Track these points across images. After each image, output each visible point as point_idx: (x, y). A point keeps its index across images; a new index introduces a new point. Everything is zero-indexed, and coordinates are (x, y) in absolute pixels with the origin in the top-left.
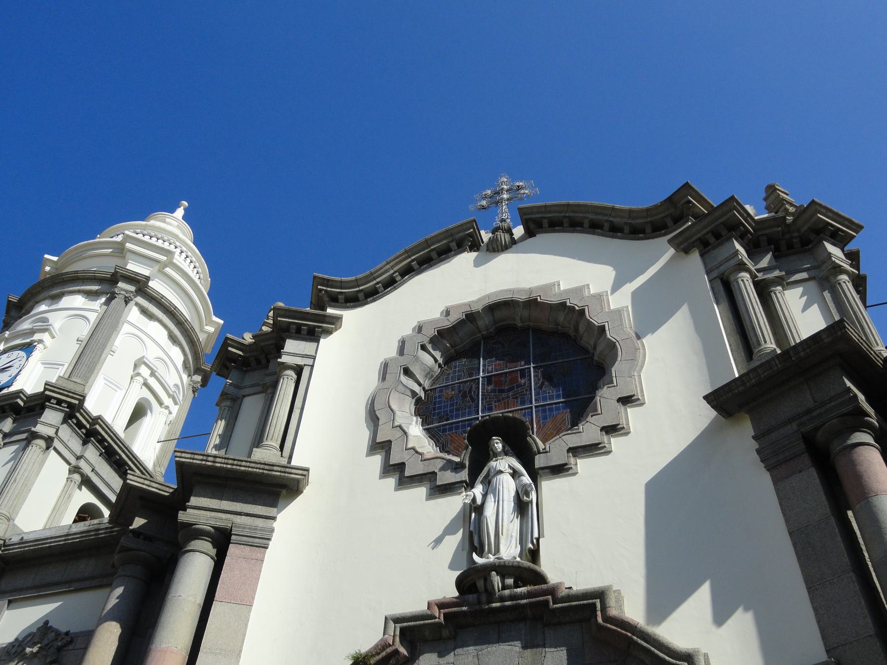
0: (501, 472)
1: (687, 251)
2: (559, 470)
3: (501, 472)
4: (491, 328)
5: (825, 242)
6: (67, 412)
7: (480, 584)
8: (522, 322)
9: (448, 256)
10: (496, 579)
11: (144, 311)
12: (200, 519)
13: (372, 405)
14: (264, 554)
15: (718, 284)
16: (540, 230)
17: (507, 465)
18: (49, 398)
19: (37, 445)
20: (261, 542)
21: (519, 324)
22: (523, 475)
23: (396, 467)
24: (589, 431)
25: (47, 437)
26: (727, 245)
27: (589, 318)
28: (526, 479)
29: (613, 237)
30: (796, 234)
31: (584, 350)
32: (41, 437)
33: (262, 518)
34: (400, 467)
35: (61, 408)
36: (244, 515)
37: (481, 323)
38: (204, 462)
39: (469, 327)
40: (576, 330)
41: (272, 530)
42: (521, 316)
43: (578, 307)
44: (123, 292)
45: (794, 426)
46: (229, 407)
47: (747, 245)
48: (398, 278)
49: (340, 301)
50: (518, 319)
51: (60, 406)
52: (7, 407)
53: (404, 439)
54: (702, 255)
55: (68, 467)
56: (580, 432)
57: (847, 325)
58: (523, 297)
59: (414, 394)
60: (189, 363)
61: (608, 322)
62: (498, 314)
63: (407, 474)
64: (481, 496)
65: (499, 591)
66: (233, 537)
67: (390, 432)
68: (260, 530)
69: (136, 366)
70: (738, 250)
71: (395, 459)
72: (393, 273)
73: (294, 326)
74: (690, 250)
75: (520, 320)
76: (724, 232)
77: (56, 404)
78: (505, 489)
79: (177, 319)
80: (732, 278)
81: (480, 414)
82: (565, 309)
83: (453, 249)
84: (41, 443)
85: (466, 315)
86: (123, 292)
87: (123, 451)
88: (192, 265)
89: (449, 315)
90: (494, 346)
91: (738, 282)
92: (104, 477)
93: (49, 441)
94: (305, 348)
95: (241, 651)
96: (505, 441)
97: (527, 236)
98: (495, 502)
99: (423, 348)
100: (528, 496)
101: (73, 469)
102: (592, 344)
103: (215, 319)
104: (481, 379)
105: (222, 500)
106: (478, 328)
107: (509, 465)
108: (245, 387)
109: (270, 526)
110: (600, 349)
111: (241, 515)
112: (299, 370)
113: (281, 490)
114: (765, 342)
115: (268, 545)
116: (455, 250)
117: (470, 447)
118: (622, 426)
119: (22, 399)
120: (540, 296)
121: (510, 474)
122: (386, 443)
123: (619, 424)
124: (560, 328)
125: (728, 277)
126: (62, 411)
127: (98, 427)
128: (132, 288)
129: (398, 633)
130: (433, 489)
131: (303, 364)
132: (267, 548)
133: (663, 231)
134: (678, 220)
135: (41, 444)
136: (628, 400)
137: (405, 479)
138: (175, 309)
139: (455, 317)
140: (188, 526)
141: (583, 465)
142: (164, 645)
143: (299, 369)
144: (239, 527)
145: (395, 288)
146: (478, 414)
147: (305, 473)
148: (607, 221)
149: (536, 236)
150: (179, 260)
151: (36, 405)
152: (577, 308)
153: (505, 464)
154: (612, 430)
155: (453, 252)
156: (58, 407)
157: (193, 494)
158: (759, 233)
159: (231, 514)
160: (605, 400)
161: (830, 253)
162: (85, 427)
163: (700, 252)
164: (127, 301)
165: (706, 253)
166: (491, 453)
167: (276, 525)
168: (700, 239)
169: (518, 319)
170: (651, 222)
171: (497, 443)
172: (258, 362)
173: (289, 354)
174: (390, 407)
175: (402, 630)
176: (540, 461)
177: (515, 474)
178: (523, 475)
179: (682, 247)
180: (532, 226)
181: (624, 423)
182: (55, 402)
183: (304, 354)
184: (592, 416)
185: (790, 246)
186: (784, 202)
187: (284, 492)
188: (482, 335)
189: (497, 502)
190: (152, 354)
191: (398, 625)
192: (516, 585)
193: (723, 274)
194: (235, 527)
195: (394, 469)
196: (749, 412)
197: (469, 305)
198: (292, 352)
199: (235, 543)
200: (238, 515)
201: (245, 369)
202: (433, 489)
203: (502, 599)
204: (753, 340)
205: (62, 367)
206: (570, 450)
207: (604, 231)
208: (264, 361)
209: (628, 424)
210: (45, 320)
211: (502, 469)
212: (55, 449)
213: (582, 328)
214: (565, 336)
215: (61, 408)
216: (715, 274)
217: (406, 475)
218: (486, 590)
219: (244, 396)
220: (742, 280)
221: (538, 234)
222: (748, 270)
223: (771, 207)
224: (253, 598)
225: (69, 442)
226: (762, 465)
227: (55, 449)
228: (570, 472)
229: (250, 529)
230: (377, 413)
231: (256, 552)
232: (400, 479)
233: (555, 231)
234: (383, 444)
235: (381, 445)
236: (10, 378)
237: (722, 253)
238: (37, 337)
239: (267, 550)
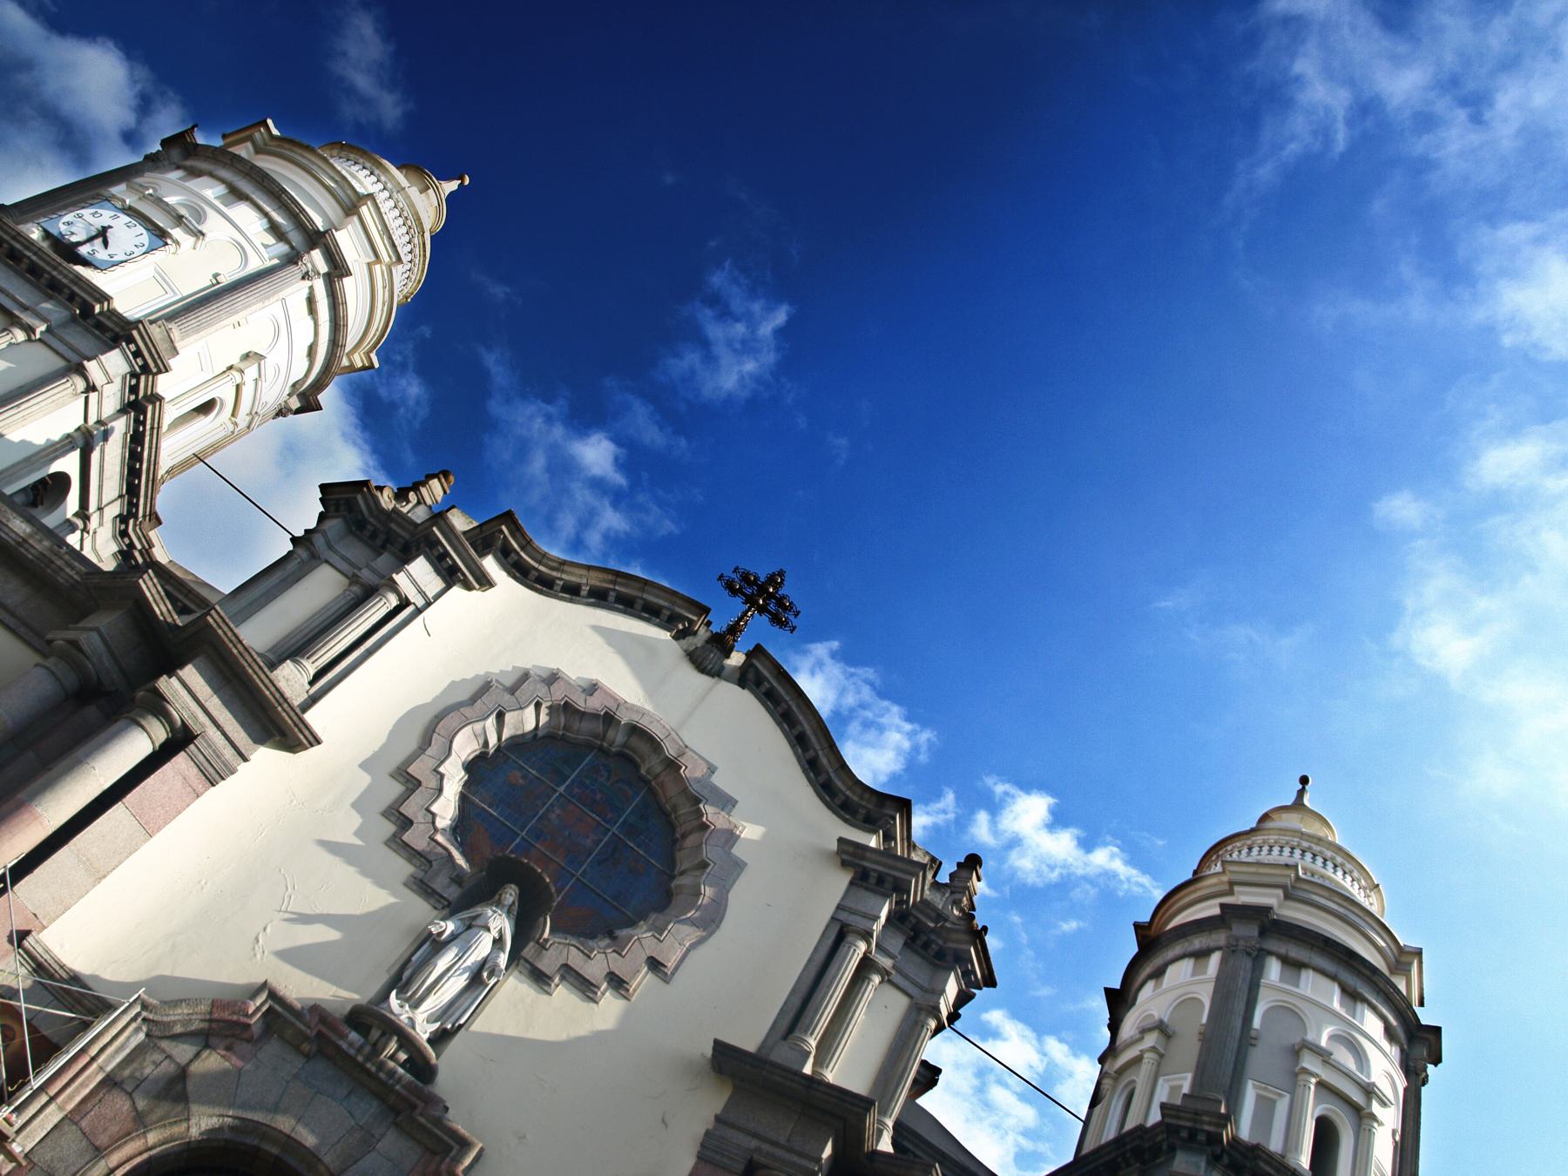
0: (488, 930)
1: (844, 864)
2: (540, 979)
3: (488, 930)
5: (953, 973)
6: (135, 370)
7: (375, 1034)
9: (651, 619)
10: (393, 1046)
11: (311, 301)
12: (177, 701)
13: (437, 720)
14: (206, 790)
15: (836, 928)
16: (754, 687)
17: (499, 928)
18: (130, 340)
19: (73, 384)
20: (213, 775)
21: (643, 772)
22: (504, 952)
23: (402, 818)
24: (595, 967)
25: (92, 384)
26: (878, 899)
27: (704, 841)
28: (503, 959)
29: (804, 771)
30: (940, 942)
31: (672, 862)
32: (86, 379)
33: (235, 750)
34: (406, 823)
35: (133, 361)
36: (221, 731)
37: (611, 734)
38: (231, 645)
39: (599, 728)
40: (684, 836)
41: (233, 772)
42: (652, 767)
43: (707, 819)
44: (309, 265)
45: (754, 1143)
46: (302, 560)
47: (896, 913)
49: (509, 559)
51: (135, 358)
52: (77, 299)
53: (434, 795)
54: (851, 883)
55: (82, 422)
56: (589, 957)
57: (872, 1111)
58: (670, 750)
59: (486, 744)
60: (302, 386)
61: (715, 864)
63: (405, 838)
64: (448, 936)
65: (385, 1057)
66: (192, 747)
67: (428, 772)
68: (223, 762)
69: (247, 356)
70: (879, 917)
71: (409, 809)
73: (441, 551)
74: (848, 865)
76: (888, 885)
77: (132, 353)
78: (476, 951)
80: (850, 938)
81: (525, 832)
82: (694, 805)
83: (662, 617)
84: (80, 384)
85: (606, 712)
86: (309, 265)
87: (150, 448)
88: (409, 247)
89: (592, 695)
90: (601, 768)
91: (850, 947)
92: (106, 458)
93: (91, 388)
94: (430, 583)
95: (105, 876)
96: (522, 897)
97: (737, 675)
98: (456, 955)
99: (538, 706)
100: (489, 977)
101: (84, 430)
102: (683, 868)
103: (373, 356)
104: (557, 794)
105: (215, 693)
106: (604, 736)
107: (501, 929)
108: (336, 552)
109: (236, 765)
110: (682, 882)
111: (218, 729)
112: (404, 603)
113: (277, 734)
114: (812, 1034)
115: (217, 783)
116: (662, 620)
117: (484, 873)
118: (628, 987)
119: (102, 308)
120: (686, 767)
122: (414, 781)
123: (628, 984)
124: (673, 816)
125: (848, 932)
126: (131, 365)
127: (150, 408)
128: (323, 267)
129: (264, 1009)
130: (415, 878)
131: (412, 601)
132: (213, 785)
133: (848, 817)
134: (869, 823)
135: (78, 386)
137: (399, 841)
138: (344, 326)
139: (594, 704)
140: (161, 697)
141: (562, 993)
142: (39, 810)
143: (404, 603)
144: (206, 741)
145: (571, 601)
146: (522, 831)
148: (815, 750)
149: (744, 689)
150: (398, 271)
151: (112, 330)
152: (704, 819)
153: (500, 922)
154: (618, 983)
155: (658, 620)
156: (131, 358)
157: (195, 662)
158: (914, 912)
159: (211, 720)
160: (640, 946)
161: (944, 991)
162: (137, 395)
163: (853, 878)
164: (306, 276)
165: (856, 885)
166: (497, 897)
167: (243, 767)
168: (864, 868)
169: (647, 766)
170: (847, 797)
171: (511, 895)
172: (374, 536)
173: (409, 576)
174: (451, 742)
175: (270, 1009)
176: (529, 951)
177: (498, 942)
178: (504, 952)
179: (844, 857)
180: (751, 676)
181: (633, 986)
182: (133, 350)
183: (424, 589)
184: (614, 951)
185: (926, 946)
186: (967, 892)
187: (278, 738)
188: (602, 745)
189: (457, 958)
190: (276, 359)
191: (270, 1002)
192: (403, 1065)
194: (203, 737)
195: (399, 818)
196: (735, 1087)
197: (620, 703)
198: (414, 577)
199: (188, 754)
201: (354, 529)
202: (415, 878)
203: (381, 1065)
204: (804, 1021)
205: (172, 294)
206: (566, 966)
207: (804, 756)
208: (379, 542)
209: (635, 990)
210: (200, 216)
211: (492, 929)
212: (87, 399)
213: (690, 841)
214: (672, 827)
215: (133, 361)
216: (843, 916)
217: (403, 838)
218: (375, 1045)
219: (327, 562)
220: (855, 950)
221: (748, 689)
222: (869, 944)
224: (159, 829)
225: (107, 400)
226: (697, 1148)
227: (87, 399)
228: (546, 988)
229: (214, 752)
230: (435, 736)
232: (394, 835)
233: (764, 704)
234: (411, 779)
235: (408, 777)
236: (108, 258)
237: (866, 900)
238: (177, 233)
239: (213, 788)
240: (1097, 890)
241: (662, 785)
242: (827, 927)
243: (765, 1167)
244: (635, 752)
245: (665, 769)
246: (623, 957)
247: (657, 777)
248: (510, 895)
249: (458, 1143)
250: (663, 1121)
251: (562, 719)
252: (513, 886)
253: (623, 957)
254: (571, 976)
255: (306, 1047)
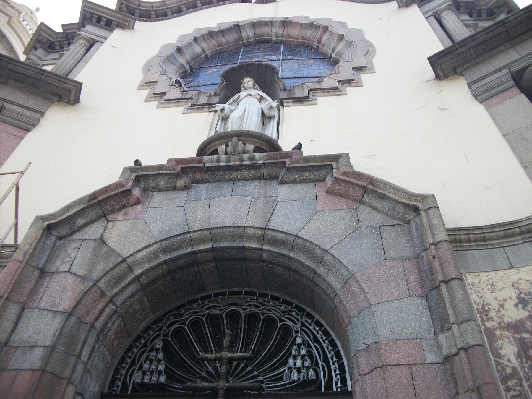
2: (300, 100)
4: (251, 39)
8: (277, 37)
15: (433, 19)
21: (274, 39)
30: (484, 8)
37: (244, 34)
48: (184, 9)
50: (274, 35)
54: (419, 7)
62: (259, 31)
72: (181, 5)
75: (276, 35)
79: (72, 273)
121: (257, 99)
136: (362, 70)
145: (181, 16)
147: (78, 85)
165: (422, 6)
193: (436, 12)
200: (11, 103)
201: (50, 50)
223: (281, 378)
231: (20, 133)
240: (498, 329)
241: (289, 36)
242: (428, 22)
243: (525, 69)
244: (263, 36)
245: (284, 28)
246: (339, 73)
247: (283, 36)
248: (248, 82)
249: (332, 161)
250: (441, 109)
251: (214, 41)
252: (247, 80)
253: (339, 73)
254: (318, 93)
255: (180, 183)
